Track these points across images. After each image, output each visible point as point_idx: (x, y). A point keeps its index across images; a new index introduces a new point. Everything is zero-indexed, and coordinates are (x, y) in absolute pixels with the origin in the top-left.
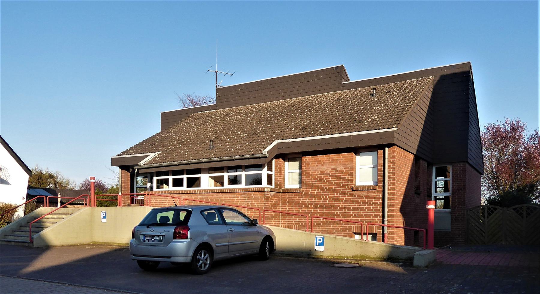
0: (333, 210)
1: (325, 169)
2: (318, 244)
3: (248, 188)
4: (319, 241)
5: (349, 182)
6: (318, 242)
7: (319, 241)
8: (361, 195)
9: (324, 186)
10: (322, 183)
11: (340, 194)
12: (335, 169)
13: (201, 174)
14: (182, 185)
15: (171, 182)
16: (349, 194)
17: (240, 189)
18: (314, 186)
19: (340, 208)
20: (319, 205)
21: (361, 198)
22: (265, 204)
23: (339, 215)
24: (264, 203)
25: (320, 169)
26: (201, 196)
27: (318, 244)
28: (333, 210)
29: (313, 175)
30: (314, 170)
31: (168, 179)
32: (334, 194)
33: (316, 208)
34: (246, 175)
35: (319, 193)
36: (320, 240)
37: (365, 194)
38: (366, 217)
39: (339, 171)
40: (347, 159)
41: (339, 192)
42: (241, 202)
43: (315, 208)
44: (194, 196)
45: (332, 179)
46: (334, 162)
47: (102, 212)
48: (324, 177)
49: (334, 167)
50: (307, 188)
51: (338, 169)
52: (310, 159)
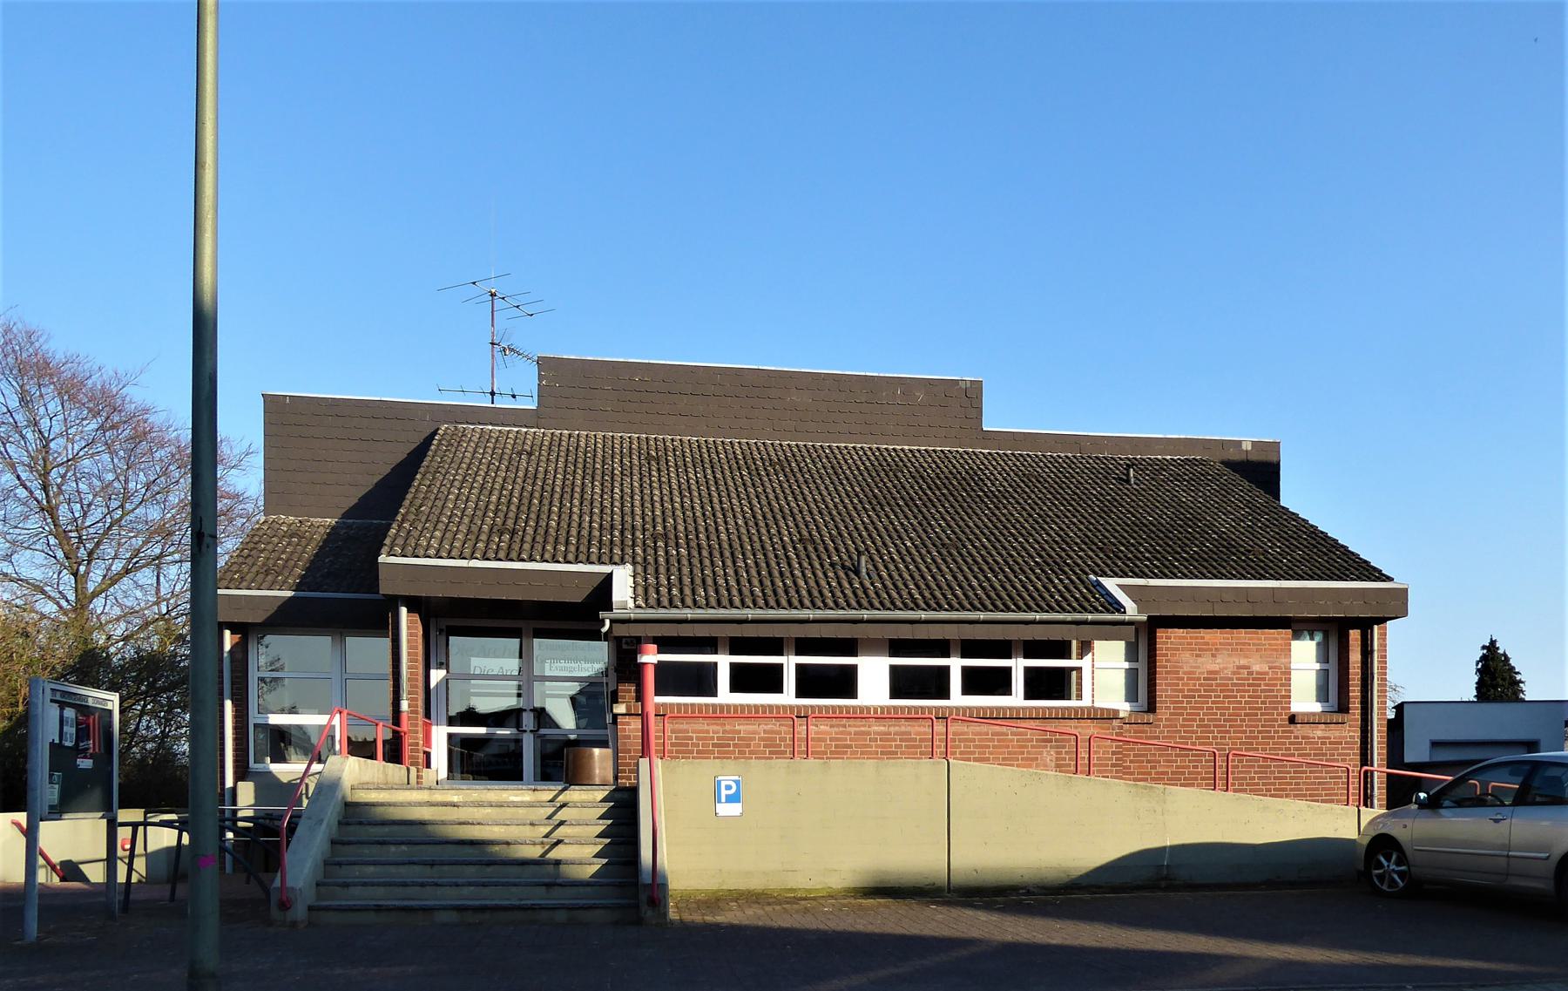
0: (1242, 772)
1: (1221, 666)
2: (723, 799)
3: (1031, 708)
4: (726, 789)
5: (1281, 703)
6: (724, 792)
7: (726, 789)
8: (1311, 735)
9: (1217, 708)
10: (1213, 702)
11: (1259, 732)
12: (1248, 668)
13: (859, 658)
14: (777, 687)
15: (790, 680)
16: (1283, 732)
17: (1010, 709)
18: (1191, 708)
19: (1259, 767)
20: (848, 737)
21: (1312, 743)
22: (1113, 753)
23: (1258, 784)
24: (1054, 743)
25: (1208, 664)
26: (885, 726)
27: (723, 799)
28: (1242, 772)
29: (1189, 679)
30: (1191, 667)
31: (949, 667)
32: (1245, 732)
33: (1196, 767)
34: (1028, 670)
35: (1206, 726)
36: (728, 787)
37: (1320, 732)
38: (1323, 789)
39: (1258, 673)
40: (1276, 645)
41: (1257, 726)
42: (1032, 747)
43: (1194, 767)
44: (855, 726)
45: (1238, 691)
46: (1241, 649)
47: (720, 778)
48: (1217, 685)
49: (1243, 662)
50: (1171, 714)
51: (1256, 668)
52: (1180, 638)
